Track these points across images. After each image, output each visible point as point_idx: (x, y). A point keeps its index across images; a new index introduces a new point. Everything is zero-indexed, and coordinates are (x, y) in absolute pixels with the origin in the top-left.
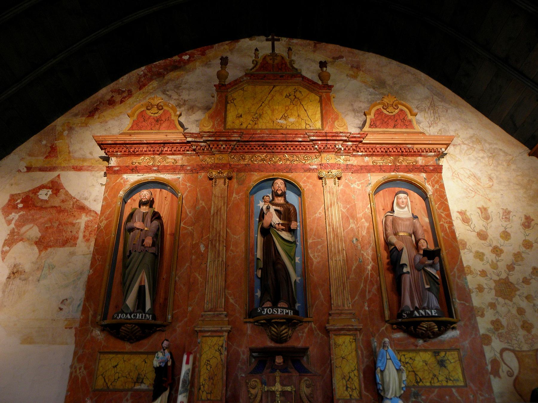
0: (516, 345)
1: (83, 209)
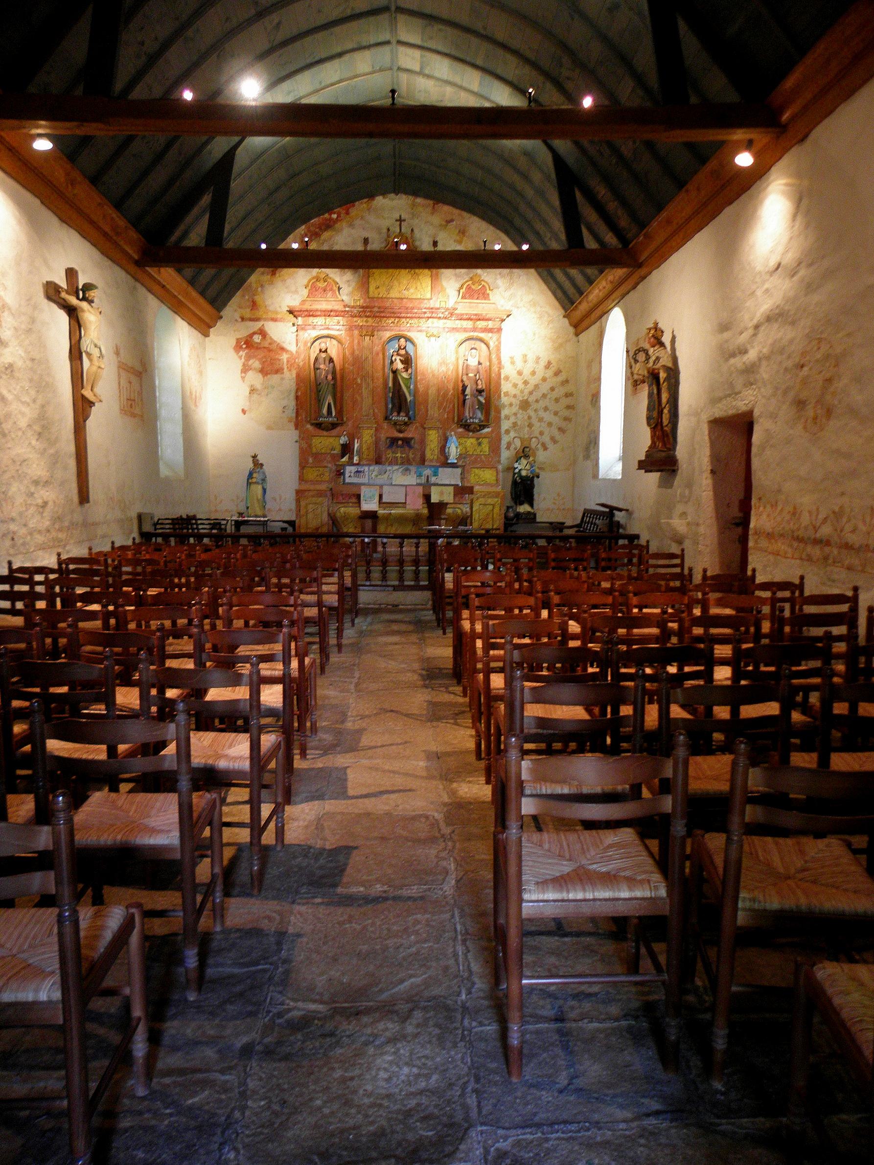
1: (283, 349)
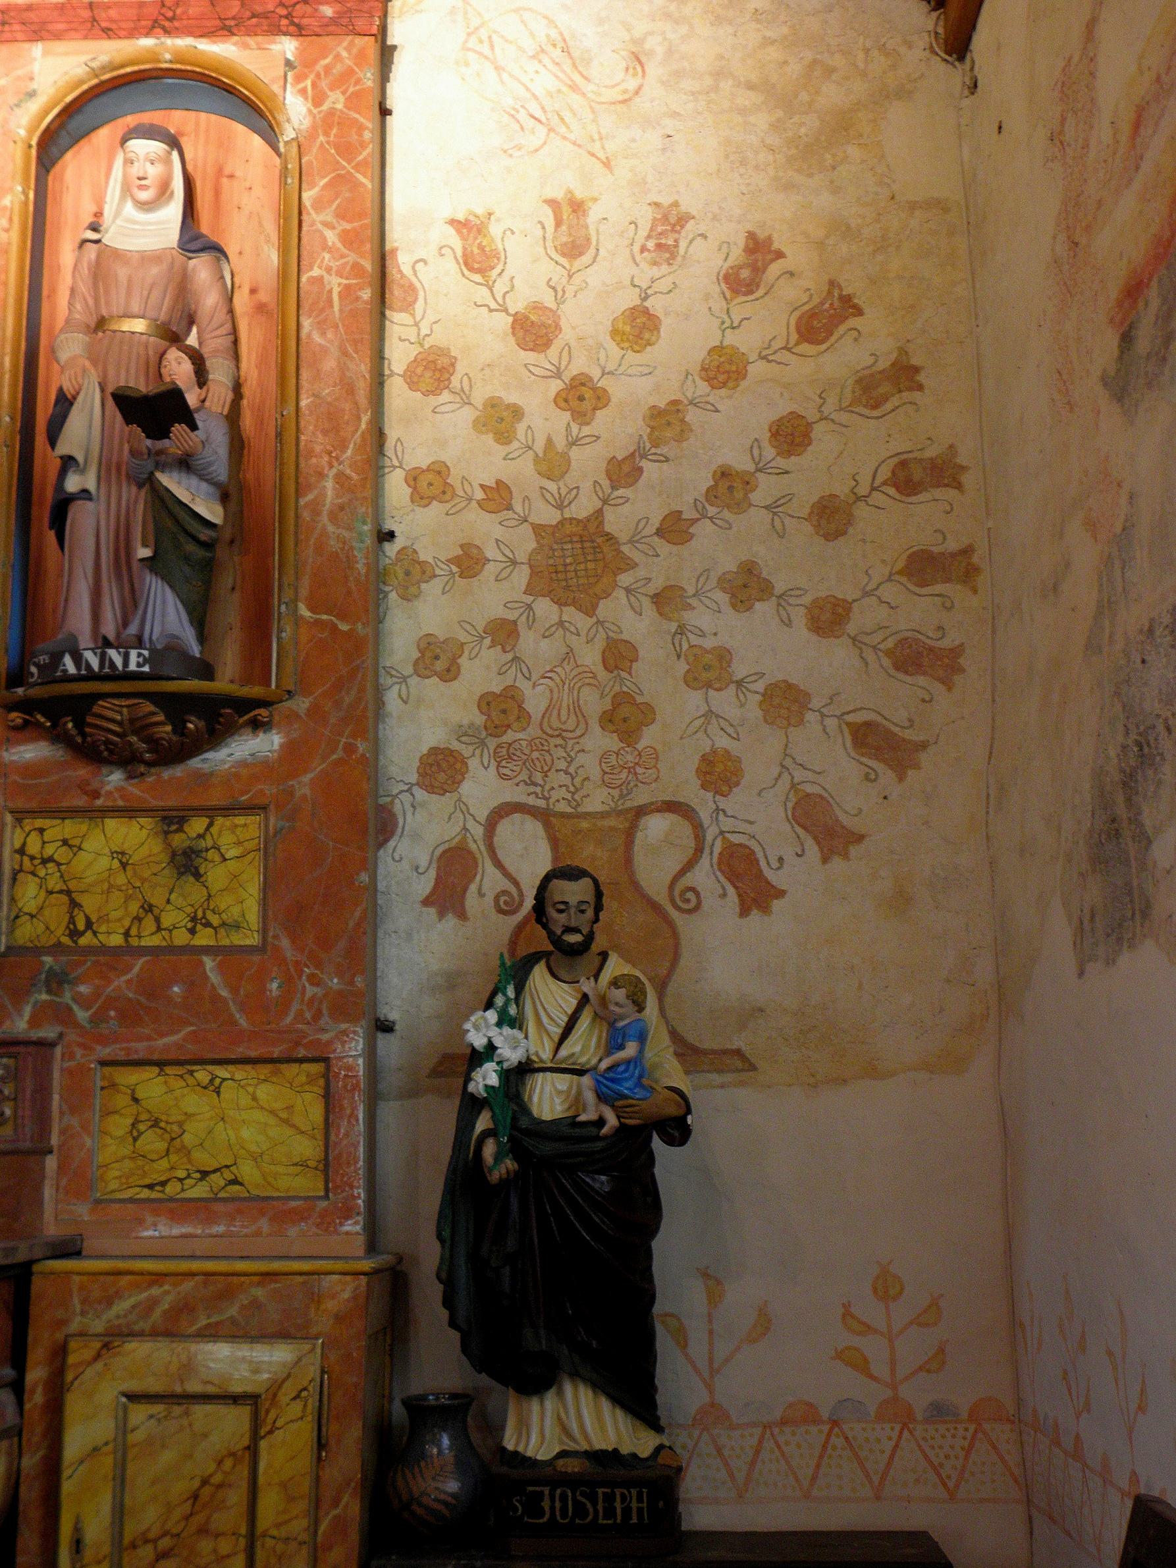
0: (563, 793)
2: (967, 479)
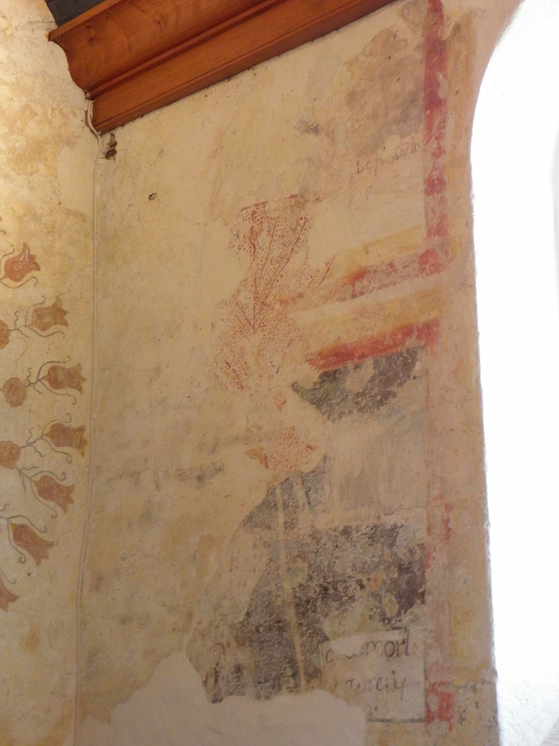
2: (86, 386)
